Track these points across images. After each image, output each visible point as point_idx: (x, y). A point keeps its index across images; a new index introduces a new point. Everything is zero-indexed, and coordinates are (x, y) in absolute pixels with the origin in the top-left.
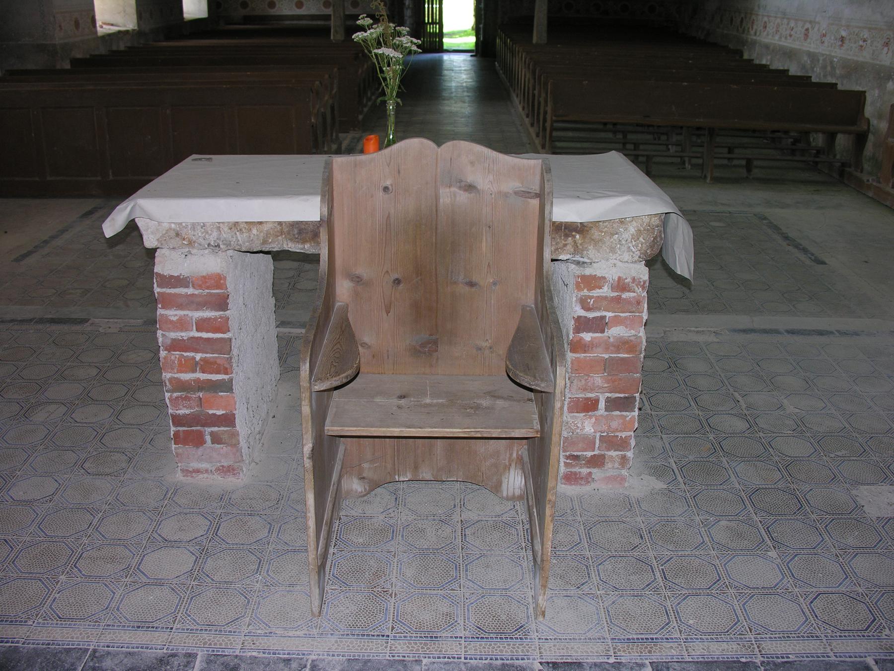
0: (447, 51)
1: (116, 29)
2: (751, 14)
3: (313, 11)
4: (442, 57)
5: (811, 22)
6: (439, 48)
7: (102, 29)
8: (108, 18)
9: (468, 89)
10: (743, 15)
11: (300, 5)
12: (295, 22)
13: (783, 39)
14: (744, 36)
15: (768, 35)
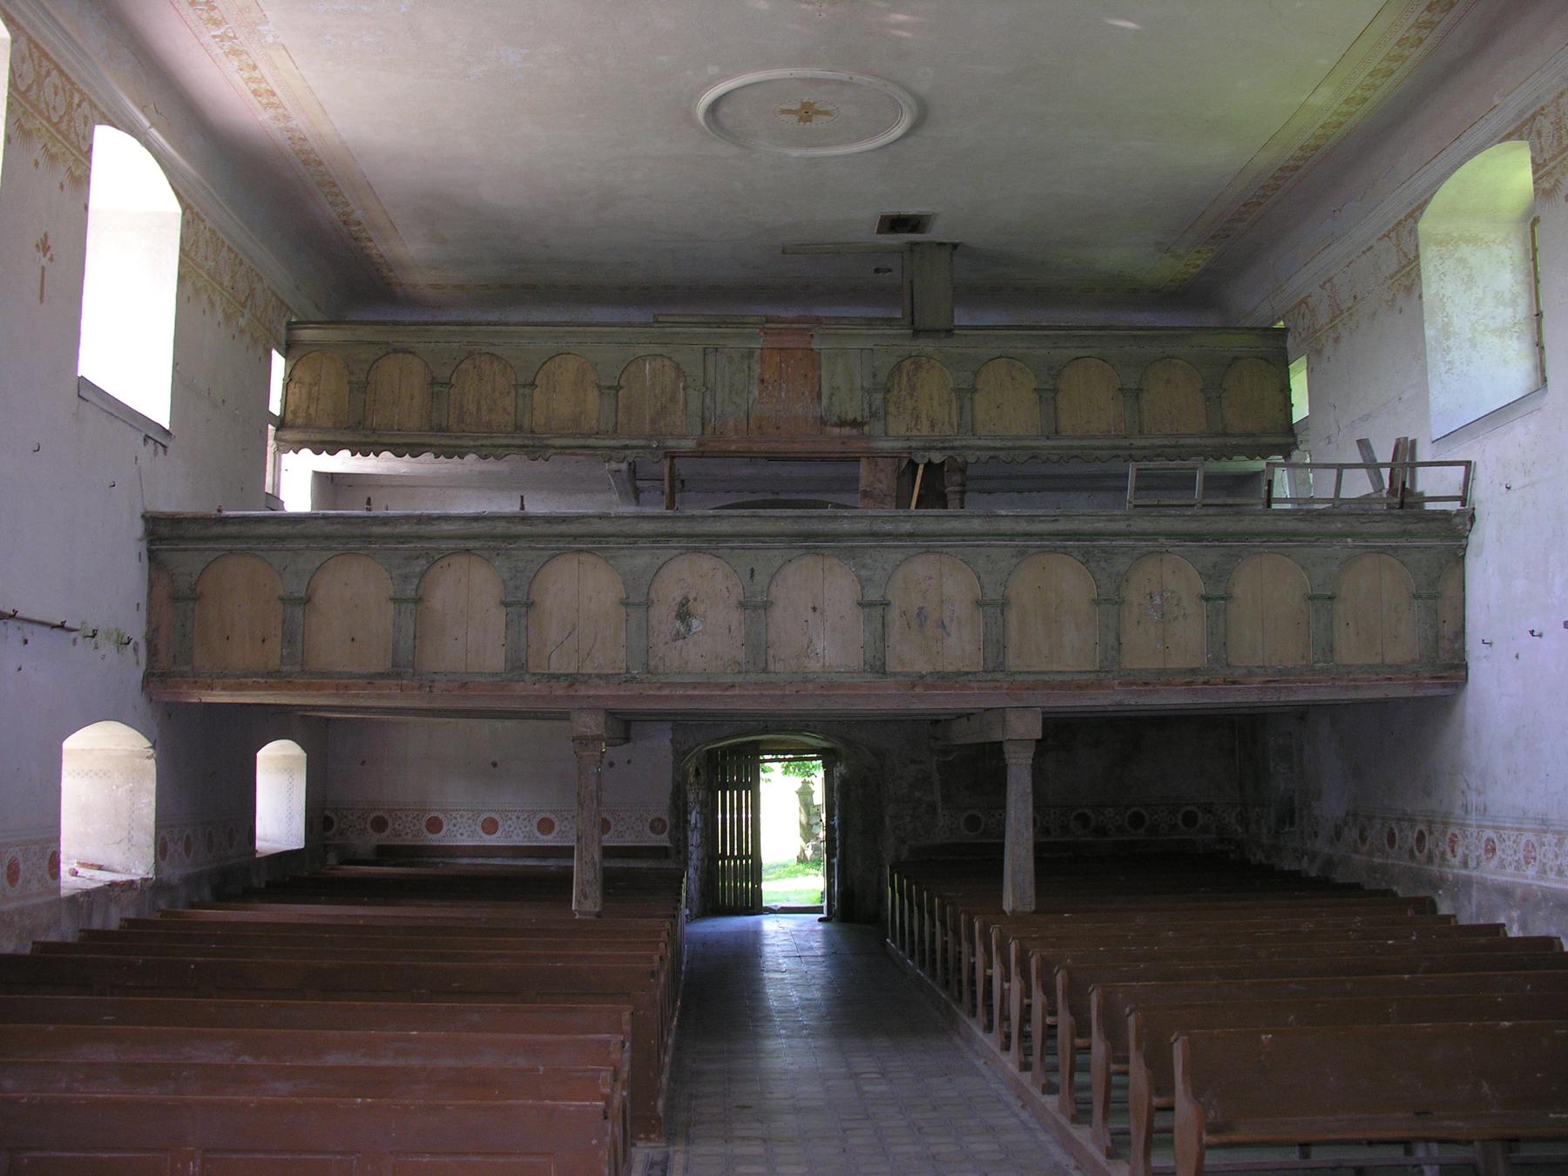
0: (771, 911)
1: (107, 877)
2: (1446, 824)
3: (518, 840)
4: (759, 923)
5: (1495, 828)
6: (754, 906)
7: (74, 877)
8: (94, 853)
9: (807, 1005)
10: (1452, 830)
11: (490, 826)
12: (480, 861)
13: (1552, 875)
14: (1434, 869)
15: (1502, 865)
